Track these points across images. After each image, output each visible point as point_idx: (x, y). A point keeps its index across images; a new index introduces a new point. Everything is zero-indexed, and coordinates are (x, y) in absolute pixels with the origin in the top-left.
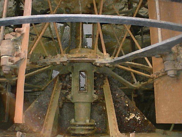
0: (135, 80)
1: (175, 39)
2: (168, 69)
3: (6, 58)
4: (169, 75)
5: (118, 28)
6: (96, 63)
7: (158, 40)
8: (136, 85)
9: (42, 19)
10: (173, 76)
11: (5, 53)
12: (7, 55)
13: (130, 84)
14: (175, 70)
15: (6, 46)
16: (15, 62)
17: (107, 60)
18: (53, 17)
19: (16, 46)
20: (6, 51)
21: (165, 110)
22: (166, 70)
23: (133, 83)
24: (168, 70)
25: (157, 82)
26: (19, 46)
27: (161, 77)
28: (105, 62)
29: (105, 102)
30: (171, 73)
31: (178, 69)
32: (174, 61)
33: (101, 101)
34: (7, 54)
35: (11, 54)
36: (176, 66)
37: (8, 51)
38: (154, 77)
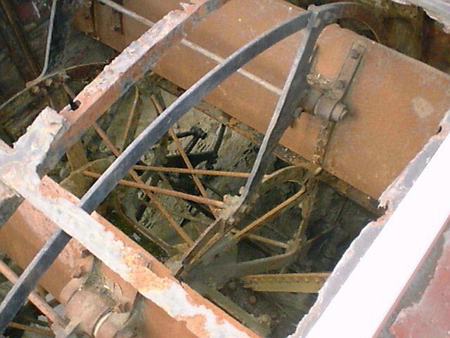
0: (282, 244)
1: (304, 48)
2: (330, 112)
3: (105, 321)
4: (339, 119)
5: (155, 224)
6: (226, 223)
7: (275, 93)
8: (291, 248)
9: (138, 149)
10: (345, 112)
11: (96, 316)
12: (102, 316)
13: (282, 256)
14: (338, 103)
15: (86, 304)
16: (132, 303)
17: (237, 202)
18: (153, 130)
19: (99, 290)
20: (94, 311)
21: (386, 173)
22: (328, 116)
23: (284, 250)
24: (331, 113)
25: (329, 162)
26: (105, 286)
27: (328, 144)
28: (237, 208)
29: (307, 270)
30: (338, 112)
31: (340, 98)
32: (323, 94)
33: (278, 321)
34: (101, 314)
35: (107, 308)
36: (333, 98)
37: (97, 306)
38: (319, 160)
